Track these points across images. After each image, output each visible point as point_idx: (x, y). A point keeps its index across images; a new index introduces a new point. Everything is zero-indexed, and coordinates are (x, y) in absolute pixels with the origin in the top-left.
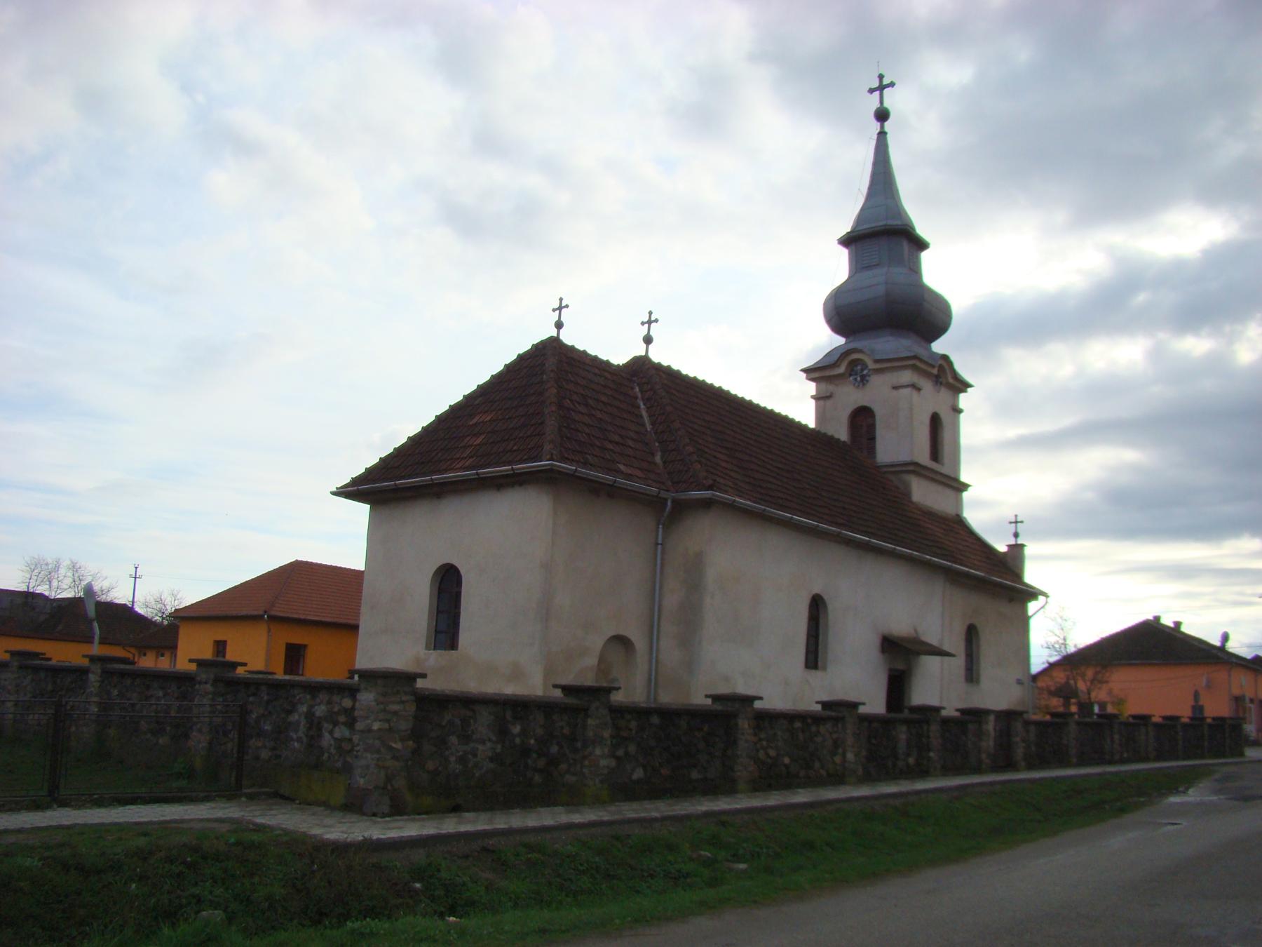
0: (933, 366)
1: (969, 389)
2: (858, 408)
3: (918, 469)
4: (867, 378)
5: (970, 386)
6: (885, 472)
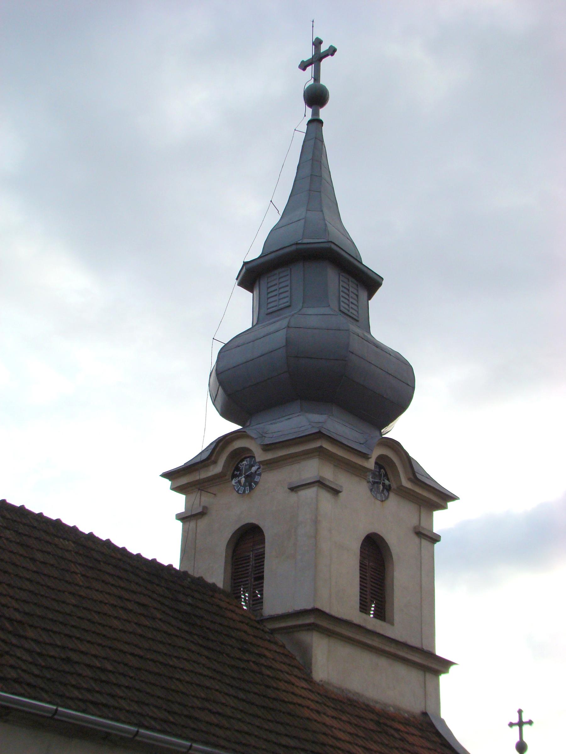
0: (366, 456)
1: (450, 504)
3: (324, 623)
4: (257, 479)
5: (452, 498)
6: (273, 631)
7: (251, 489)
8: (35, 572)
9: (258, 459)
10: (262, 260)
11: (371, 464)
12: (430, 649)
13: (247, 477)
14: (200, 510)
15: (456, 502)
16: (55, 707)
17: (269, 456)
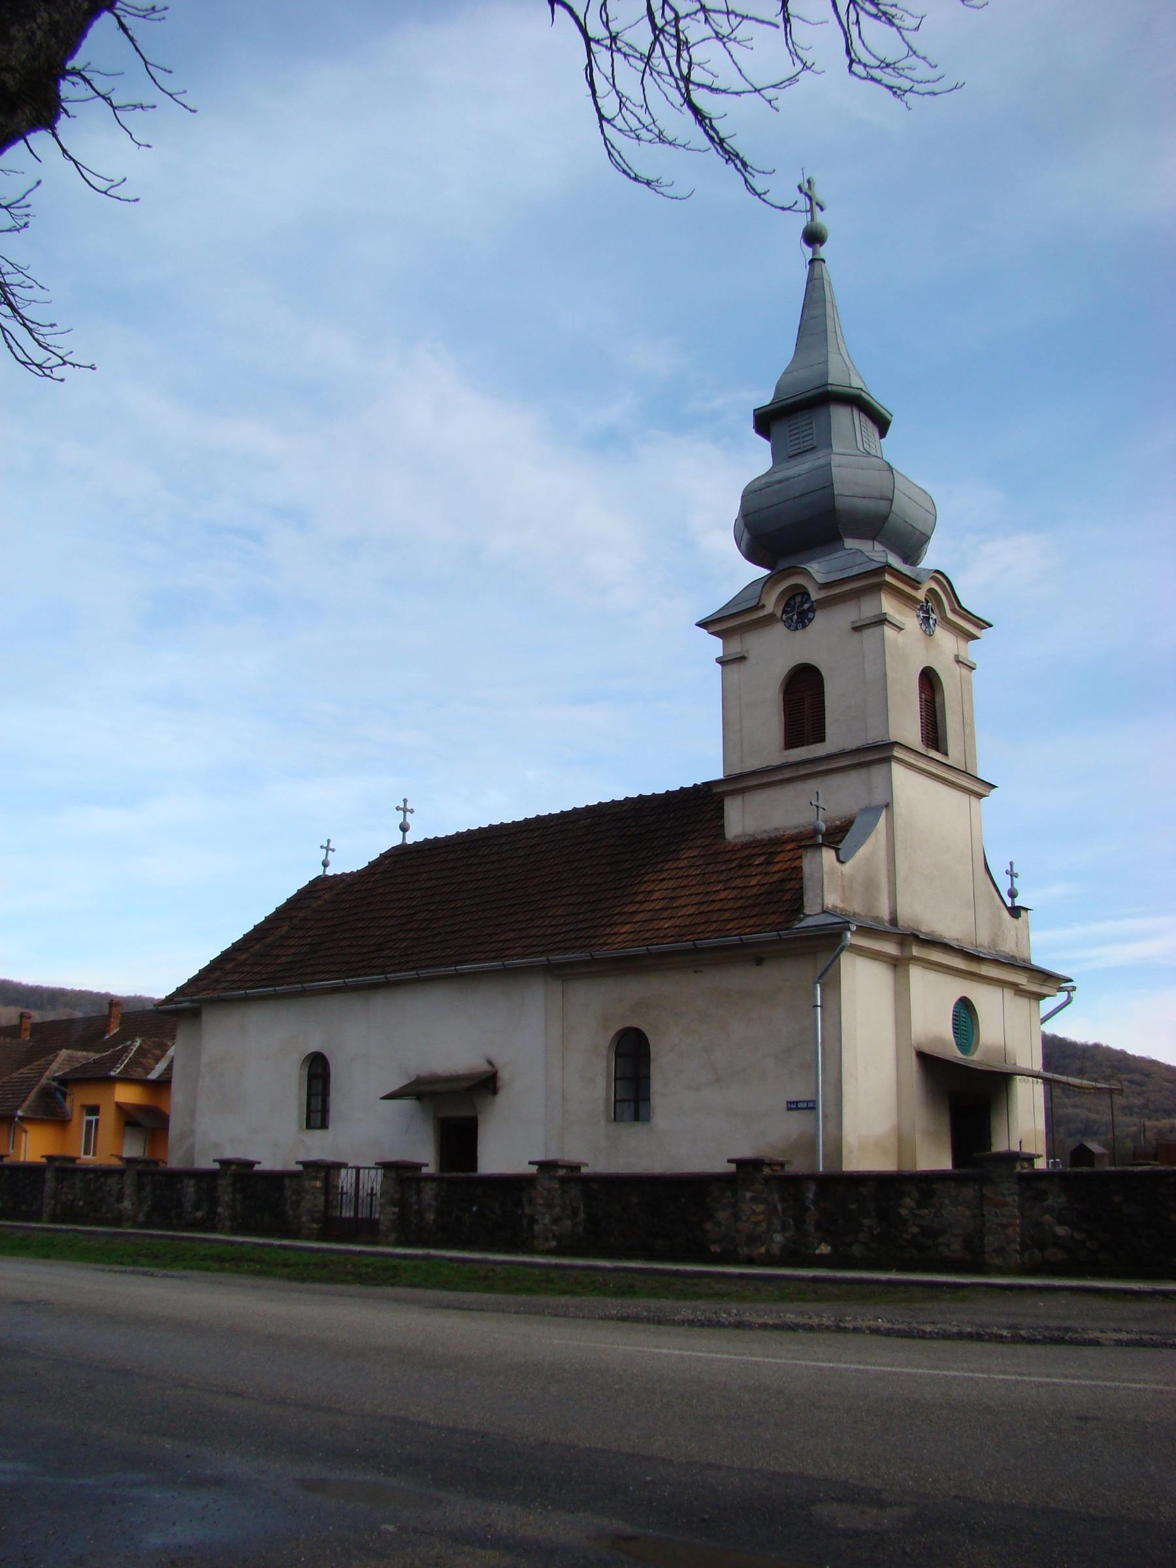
2: (791, 669)
4: (810, 615)
10: (771, 407)
11: (920, 595)
13: (799, 614)
16: (819, 1004)
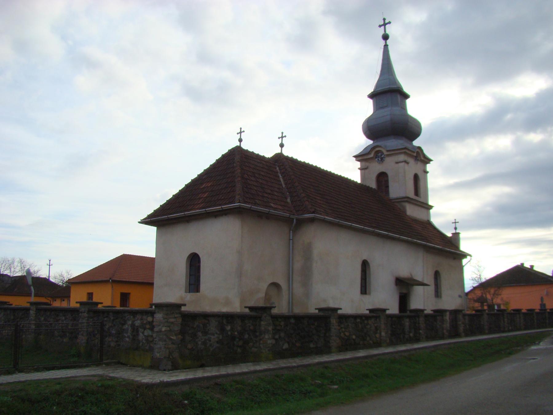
0: (414, 152)
1: (431, 162)
3: (409, 200)
4: (384, 159)
7: (382, 162)
8: (262, 167)
9: (385, 154)
12: (425, 202)
13: (381, 158)
14: (366, 167)
15: (433, 161)
17: (388, 153)
